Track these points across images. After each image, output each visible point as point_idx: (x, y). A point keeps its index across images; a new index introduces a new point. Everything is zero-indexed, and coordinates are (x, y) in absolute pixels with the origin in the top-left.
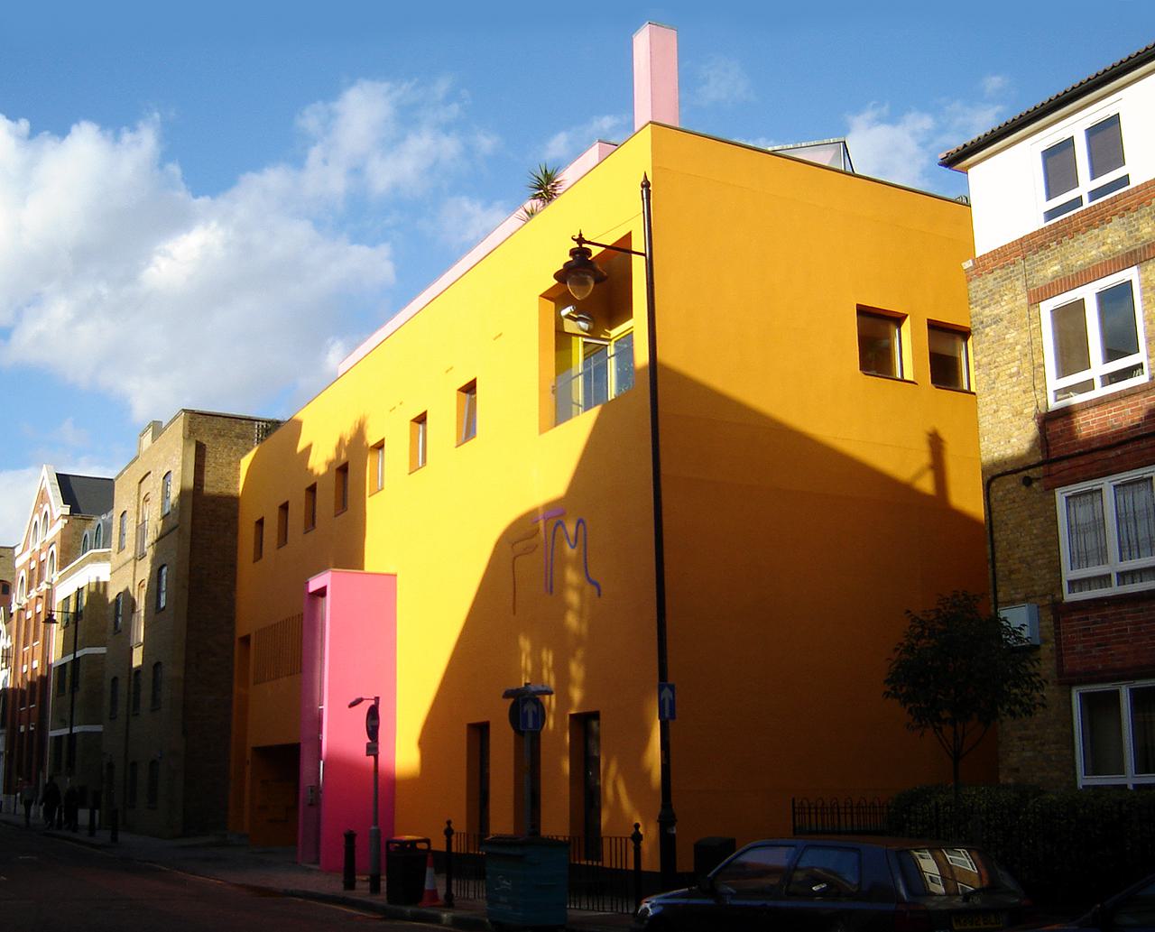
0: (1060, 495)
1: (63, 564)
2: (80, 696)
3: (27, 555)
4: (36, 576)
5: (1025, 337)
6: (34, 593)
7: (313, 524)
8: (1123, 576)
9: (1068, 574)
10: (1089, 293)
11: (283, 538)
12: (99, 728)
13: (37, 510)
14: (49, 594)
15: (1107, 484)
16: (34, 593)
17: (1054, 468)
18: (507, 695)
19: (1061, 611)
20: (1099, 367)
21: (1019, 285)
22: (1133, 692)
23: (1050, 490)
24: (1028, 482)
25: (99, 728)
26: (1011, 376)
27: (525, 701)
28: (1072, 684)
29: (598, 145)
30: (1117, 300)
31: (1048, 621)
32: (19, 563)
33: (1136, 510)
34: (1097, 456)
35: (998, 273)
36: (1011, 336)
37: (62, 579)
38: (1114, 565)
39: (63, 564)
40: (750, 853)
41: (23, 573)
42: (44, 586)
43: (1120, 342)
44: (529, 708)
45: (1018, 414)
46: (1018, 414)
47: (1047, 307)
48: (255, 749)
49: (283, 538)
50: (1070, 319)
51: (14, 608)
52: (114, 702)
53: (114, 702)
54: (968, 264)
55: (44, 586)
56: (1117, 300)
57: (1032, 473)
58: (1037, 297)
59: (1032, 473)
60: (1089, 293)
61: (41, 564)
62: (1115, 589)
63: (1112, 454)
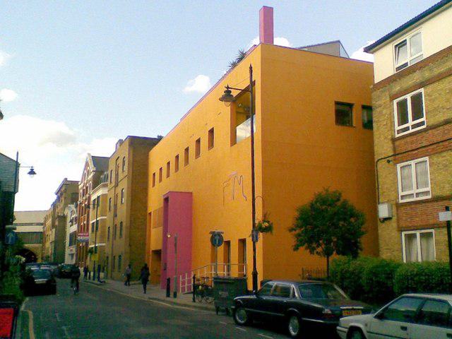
0: (399, 166)
1: (93, 188)
2: (99, 233)
3: (82, 185)
4: (85, 192)
5: (388, 113)
6: (84, 198)
7: (188, 162)
8: (418, 194)
9: (401, 193)
10: (408, 97)
11: (177, 168)
12: (104, 244)
13: (85, 169)
14: (89, 198)
15: (413, 163)
16: (84, 198)
17: (397, 156)
18: (211, 233)
19: (399, 206)
20: (411, 123)
21: (387, 93)
22: (405, 235)
23: (395, 164)
24: (389, 161)
25: (104, 244)
26: (384, 125)
27: (215, 236)
28: (402, 231)
29: (49, 254)
30: (417, 101)
31: (394, 209)
32: (80, 187)
33: (418, 172)
34: (410, 153)
35: (381, 89)
36: (384, 111)
37: (93, 193)
38: (415, 191)
39: (93, 188)
40: (392, 305)
41: (81, 191)
42: (88, 195)
43: (417, 113)
44: (217, 238)
45: (386, 138)
46: (386, 138)
47: (395, 102)
48: (153, 251)
49: (177, 168)
50: (402, 106)
51: (79, 203)
52: (121, 229)
53: (121, 229)
54: (372, 86)
55: (88, 195)
56: (417, 101)
57: (390, 159)
58: (392, 98)
59: (390, 159)
60: (408, 97)
61: (87, 188)
62: (415, 199)
63: (414, 152)
